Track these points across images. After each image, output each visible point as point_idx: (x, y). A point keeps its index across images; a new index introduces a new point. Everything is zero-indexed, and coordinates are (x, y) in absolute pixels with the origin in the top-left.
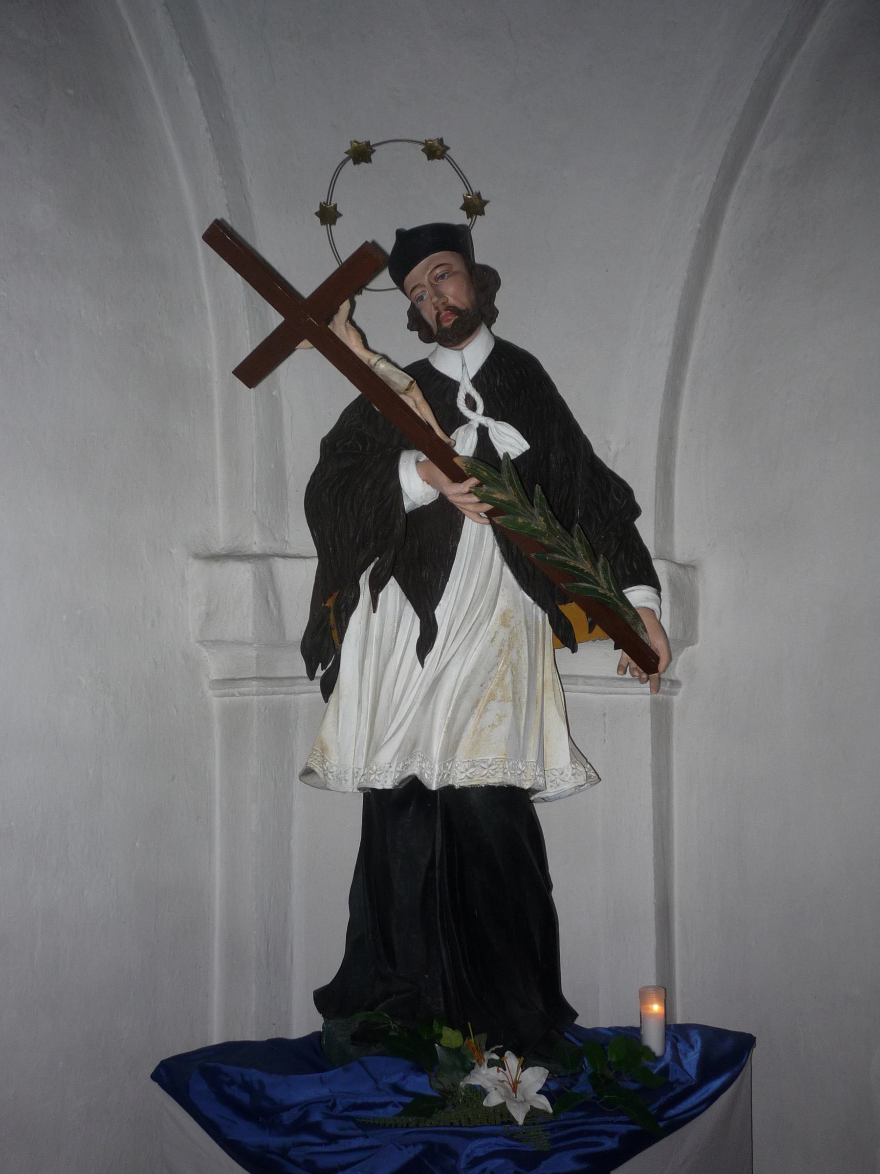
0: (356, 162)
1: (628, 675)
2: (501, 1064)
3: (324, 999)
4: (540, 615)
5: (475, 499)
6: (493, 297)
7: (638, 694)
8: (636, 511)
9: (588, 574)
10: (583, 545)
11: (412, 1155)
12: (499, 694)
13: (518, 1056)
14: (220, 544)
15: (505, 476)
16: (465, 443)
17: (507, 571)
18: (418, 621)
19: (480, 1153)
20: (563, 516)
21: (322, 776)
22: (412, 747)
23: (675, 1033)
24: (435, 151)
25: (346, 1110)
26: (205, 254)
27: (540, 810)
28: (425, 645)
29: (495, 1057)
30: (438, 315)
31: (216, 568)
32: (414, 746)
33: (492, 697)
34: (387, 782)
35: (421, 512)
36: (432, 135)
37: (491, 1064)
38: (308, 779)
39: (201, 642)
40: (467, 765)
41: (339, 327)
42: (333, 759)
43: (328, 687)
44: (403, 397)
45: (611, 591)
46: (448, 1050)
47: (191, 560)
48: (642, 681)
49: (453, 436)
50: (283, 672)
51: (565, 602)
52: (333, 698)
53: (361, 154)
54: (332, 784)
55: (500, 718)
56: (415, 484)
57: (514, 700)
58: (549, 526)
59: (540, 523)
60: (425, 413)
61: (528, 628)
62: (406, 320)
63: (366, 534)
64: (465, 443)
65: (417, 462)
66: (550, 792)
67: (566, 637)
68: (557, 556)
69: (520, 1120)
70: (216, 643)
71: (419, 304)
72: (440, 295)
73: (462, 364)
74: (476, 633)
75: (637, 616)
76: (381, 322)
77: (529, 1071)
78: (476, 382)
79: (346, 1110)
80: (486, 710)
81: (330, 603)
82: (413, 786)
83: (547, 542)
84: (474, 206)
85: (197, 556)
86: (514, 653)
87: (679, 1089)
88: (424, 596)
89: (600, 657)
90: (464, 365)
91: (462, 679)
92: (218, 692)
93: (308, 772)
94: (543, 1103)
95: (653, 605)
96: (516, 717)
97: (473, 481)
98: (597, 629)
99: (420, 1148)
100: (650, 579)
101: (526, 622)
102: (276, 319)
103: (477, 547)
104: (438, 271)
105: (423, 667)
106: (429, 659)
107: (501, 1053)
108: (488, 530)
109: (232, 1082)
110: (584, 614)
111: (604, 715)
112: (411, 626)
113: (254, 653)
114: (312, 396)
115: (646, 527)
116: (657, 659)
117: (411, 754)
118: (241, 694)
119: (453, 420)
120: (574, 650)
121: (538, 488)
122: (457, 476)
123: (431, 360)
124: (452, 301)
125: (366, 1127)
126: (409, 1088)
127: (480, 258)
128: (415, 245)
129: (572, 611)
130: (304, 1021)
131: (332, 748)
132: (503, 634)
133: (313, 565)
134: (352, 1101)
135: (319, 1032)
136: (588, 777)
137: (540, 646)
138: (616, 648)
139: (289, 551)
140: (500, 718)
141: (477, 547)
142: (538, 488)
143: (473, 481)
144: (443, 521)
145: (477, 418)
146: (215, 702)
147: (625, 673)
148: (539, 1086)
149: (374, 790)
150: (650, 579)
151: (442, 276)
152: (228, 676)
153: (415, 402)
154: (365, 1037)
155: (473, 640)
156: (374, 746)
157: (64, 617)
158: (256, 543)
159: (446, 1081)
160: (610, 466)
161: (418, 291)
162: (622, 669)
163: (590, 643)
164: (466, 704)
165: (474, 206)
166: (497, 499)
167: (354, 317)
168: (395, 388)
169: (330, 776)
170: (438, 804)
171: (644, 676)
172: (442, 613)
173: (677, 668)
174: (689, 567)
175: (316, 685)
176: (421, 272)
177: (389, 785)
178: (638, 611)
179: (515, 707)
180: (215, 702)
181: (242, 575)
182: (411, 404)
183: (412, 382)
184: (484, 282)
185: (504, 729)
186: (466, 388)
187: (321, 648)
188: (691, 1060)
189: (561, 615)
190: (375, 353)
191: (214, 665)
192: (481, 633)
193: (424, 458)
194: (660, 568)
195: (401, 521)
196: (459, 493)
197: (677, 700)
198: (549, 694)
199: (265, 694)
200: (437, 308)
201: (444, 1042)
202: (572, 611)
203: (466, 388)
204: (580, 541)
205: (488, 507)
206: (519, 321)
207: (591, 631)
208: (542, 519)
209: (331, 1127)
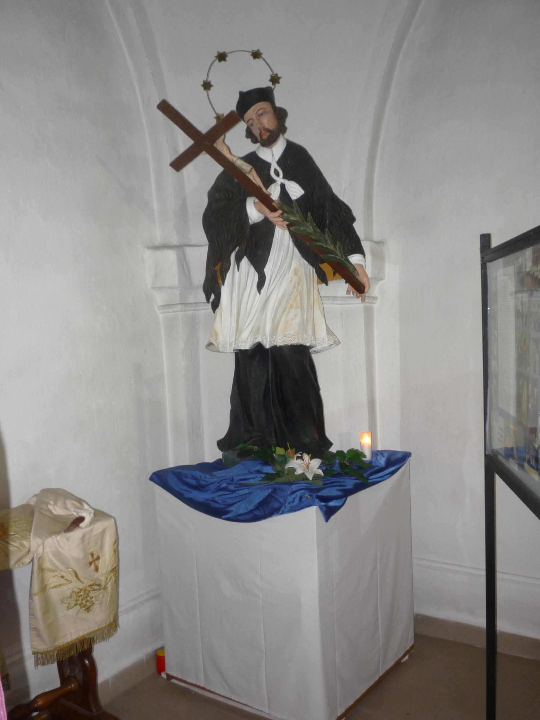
0: (220, 61)
1: (351, 295)
2: (301, 458)
3: (222, 444)
4: (312, 270)
5: (281, 219)
6: (284, 121)
7: (356, 304)
8: (353, 219)
9: (332, 251)
10: (330, 236)
11: (267, 494)
12: (295, 305)
13: (308, 454)
14: (158, 241)
15: (294, 210)
16: (274, 192)
17: (296, 250)
18: (257, 274)
19: (294, 489)
20: (321, 225)
21: (216, 345)
22: (257, 330)
23: (375, 453)
24: (256, 55)
25: (238, 481)
26: (161, 116)
27: (314, 357)
28: (260, 285)
29: (300, 455)
30: (260, 133)
31: (158, 253)
32: (258, 329)
33: (292, 307)
34: (247, 346)
35: (256, 226)
36: (255, 49)
37: (298, 458)
38: (212, 348)
39: (153, 288)
40: (282, 336)
41: (219, 145)
42: (221, 338)
43: (215, 305)
44: (248, 175)
45: (343, 258)
46: (279, 455)
47: (146, 249)
48: (357, 297)
49: (269, 190)
50: (191, 300)
51: (322, 263)
52: (218, 310)
53: (222, 57)
54: (221, 349)
55: (296, 316)
56: (254, 213)
57: (301, 308)
58: (314, 230)
59: (310, 229)
60: (256, 180)
61: (306, 276)
62: (245, 134)
63: (232, 237)
64: (274, 192)
65: (254, 202)
66: (318, 348)
67: (323, 278)
68: (319, 243)
69: (311, 478)
70: (161, 288)
71: (251, 127)
72: (261, 123)
73: (272, 155)
74: (283, 279)
75: (355, 269)
76: (237, 144)
77: (314, 460)
78: (279, 163)
79: (238, 481)
80: (289, 312)
81: (218, 268)
82: (259, 347)
83: (314, 237)
84: (275, 79)
85: (148, 248)
86: (300, 286)
87: (377, 468)
88: (259, 264)
89: (340, 287)
90: (273, 155)
91: (278, 299)
92: (162, 311)
93: (210, 344)
94: (320, 472)
95: (362, 263)
96: (302, 315)
97: (280, 212)
98: (337, 275)
99: (270, 490)
100: (360, 250)
101: (305, 273)
102: (190, 142)
103: (282, 237)
104: (260, 112)
105: (260, 294)
106: (263, 291)
107: (302, 454)
108: (287, 233)
109: (186, 477)
110: (331, 269)
111: (342, 314)
112: (254, 276)
113: (179, 292)
114: (204, 172)
115: (359, 227)
116: (364, 287)
117: (257, 333)
118: (173, 312)
119: (268, 181)
120: (327, 285)
121: (309, 214)
122: (273, 210)
123: (257, 153)
124: (267, 126)
125: (248, 486)
126: (265, 471)
127: (278, 104)
128: (247, 100)
129: (325, 267)
130: (212, 454)
131: (220, 333)
132: (295, 278)
133: (205, 250)
134: (240, 478)
135: (220, 459)
136: (335, 341)
137: (312, 283)
138: (346, 283)
139: (191, 243)
140: (296, 316)
141: (282, 237)
142: (309, 214)
143: (280, 212)
144: (266, 230)
145: (280, 180)
146: (161, 316)
147: (350, 294)
148: (318, 466)
149: (240, 350)
150: (360, 250)
151: (262, 114)
152: (166, 304)
153: (253, 177)
154: (244, 454)
155: (282, 282)
156: (238, 331)
157: (94, 280)
158: (175, 240)
159: (278, 468)
160: (341, 197)
161: (251, 122)
162: (348, 292)
163: (335, 281)
164: (280, 311)
165: (275, 79)
166: (291, 220)
167: (226, 141)
168: (244, 171)
169: (220, 345)
170: (270, 355)
171: (359, 295)
172: (268, 270)
173: (374, 290)
174: (380, 243)
175: (209, 306)
176: (251, 113)
177: (247, 347)
178: (355, 266)
179: (302, 311)
180: (161, 316)
181: (171, 256)
182: (251, 178)
183: (251, 169)
184: (281, 115)
185: (297, 320)
186: (274, 166)
187: (212, 287)
188: (382, 461)
189: (321, 269)
190: (235, 156)
191: (160, 298)
192: (285, 279)
193: (257, 200)
194: (365, 245)
195: (248, 231)
196: (273, 217)
197: (376, 306)
198: (316, 305)
199: (185, 311)
200: (260, 130)
201: (277, 453)
202: (325, 267)
203: (274, 166)
204: (328, 236)
205: (287, 223)
206: (296, 132)
207: (334, 276)
208: (311, 227)
209: (232, 487)
